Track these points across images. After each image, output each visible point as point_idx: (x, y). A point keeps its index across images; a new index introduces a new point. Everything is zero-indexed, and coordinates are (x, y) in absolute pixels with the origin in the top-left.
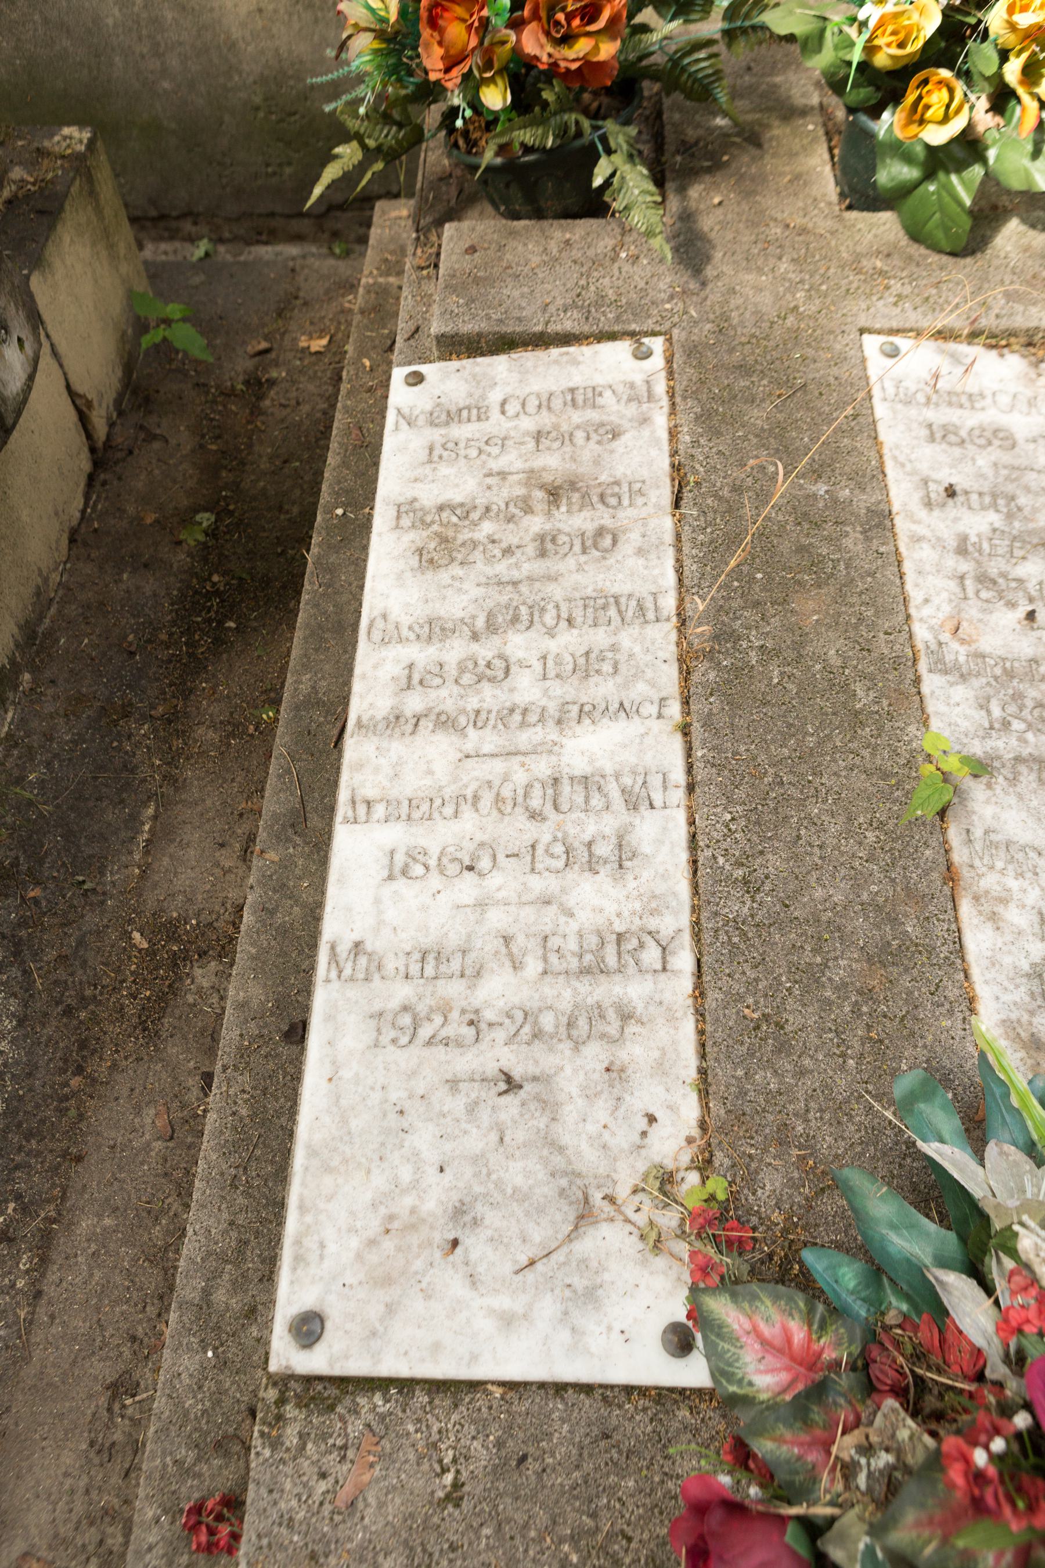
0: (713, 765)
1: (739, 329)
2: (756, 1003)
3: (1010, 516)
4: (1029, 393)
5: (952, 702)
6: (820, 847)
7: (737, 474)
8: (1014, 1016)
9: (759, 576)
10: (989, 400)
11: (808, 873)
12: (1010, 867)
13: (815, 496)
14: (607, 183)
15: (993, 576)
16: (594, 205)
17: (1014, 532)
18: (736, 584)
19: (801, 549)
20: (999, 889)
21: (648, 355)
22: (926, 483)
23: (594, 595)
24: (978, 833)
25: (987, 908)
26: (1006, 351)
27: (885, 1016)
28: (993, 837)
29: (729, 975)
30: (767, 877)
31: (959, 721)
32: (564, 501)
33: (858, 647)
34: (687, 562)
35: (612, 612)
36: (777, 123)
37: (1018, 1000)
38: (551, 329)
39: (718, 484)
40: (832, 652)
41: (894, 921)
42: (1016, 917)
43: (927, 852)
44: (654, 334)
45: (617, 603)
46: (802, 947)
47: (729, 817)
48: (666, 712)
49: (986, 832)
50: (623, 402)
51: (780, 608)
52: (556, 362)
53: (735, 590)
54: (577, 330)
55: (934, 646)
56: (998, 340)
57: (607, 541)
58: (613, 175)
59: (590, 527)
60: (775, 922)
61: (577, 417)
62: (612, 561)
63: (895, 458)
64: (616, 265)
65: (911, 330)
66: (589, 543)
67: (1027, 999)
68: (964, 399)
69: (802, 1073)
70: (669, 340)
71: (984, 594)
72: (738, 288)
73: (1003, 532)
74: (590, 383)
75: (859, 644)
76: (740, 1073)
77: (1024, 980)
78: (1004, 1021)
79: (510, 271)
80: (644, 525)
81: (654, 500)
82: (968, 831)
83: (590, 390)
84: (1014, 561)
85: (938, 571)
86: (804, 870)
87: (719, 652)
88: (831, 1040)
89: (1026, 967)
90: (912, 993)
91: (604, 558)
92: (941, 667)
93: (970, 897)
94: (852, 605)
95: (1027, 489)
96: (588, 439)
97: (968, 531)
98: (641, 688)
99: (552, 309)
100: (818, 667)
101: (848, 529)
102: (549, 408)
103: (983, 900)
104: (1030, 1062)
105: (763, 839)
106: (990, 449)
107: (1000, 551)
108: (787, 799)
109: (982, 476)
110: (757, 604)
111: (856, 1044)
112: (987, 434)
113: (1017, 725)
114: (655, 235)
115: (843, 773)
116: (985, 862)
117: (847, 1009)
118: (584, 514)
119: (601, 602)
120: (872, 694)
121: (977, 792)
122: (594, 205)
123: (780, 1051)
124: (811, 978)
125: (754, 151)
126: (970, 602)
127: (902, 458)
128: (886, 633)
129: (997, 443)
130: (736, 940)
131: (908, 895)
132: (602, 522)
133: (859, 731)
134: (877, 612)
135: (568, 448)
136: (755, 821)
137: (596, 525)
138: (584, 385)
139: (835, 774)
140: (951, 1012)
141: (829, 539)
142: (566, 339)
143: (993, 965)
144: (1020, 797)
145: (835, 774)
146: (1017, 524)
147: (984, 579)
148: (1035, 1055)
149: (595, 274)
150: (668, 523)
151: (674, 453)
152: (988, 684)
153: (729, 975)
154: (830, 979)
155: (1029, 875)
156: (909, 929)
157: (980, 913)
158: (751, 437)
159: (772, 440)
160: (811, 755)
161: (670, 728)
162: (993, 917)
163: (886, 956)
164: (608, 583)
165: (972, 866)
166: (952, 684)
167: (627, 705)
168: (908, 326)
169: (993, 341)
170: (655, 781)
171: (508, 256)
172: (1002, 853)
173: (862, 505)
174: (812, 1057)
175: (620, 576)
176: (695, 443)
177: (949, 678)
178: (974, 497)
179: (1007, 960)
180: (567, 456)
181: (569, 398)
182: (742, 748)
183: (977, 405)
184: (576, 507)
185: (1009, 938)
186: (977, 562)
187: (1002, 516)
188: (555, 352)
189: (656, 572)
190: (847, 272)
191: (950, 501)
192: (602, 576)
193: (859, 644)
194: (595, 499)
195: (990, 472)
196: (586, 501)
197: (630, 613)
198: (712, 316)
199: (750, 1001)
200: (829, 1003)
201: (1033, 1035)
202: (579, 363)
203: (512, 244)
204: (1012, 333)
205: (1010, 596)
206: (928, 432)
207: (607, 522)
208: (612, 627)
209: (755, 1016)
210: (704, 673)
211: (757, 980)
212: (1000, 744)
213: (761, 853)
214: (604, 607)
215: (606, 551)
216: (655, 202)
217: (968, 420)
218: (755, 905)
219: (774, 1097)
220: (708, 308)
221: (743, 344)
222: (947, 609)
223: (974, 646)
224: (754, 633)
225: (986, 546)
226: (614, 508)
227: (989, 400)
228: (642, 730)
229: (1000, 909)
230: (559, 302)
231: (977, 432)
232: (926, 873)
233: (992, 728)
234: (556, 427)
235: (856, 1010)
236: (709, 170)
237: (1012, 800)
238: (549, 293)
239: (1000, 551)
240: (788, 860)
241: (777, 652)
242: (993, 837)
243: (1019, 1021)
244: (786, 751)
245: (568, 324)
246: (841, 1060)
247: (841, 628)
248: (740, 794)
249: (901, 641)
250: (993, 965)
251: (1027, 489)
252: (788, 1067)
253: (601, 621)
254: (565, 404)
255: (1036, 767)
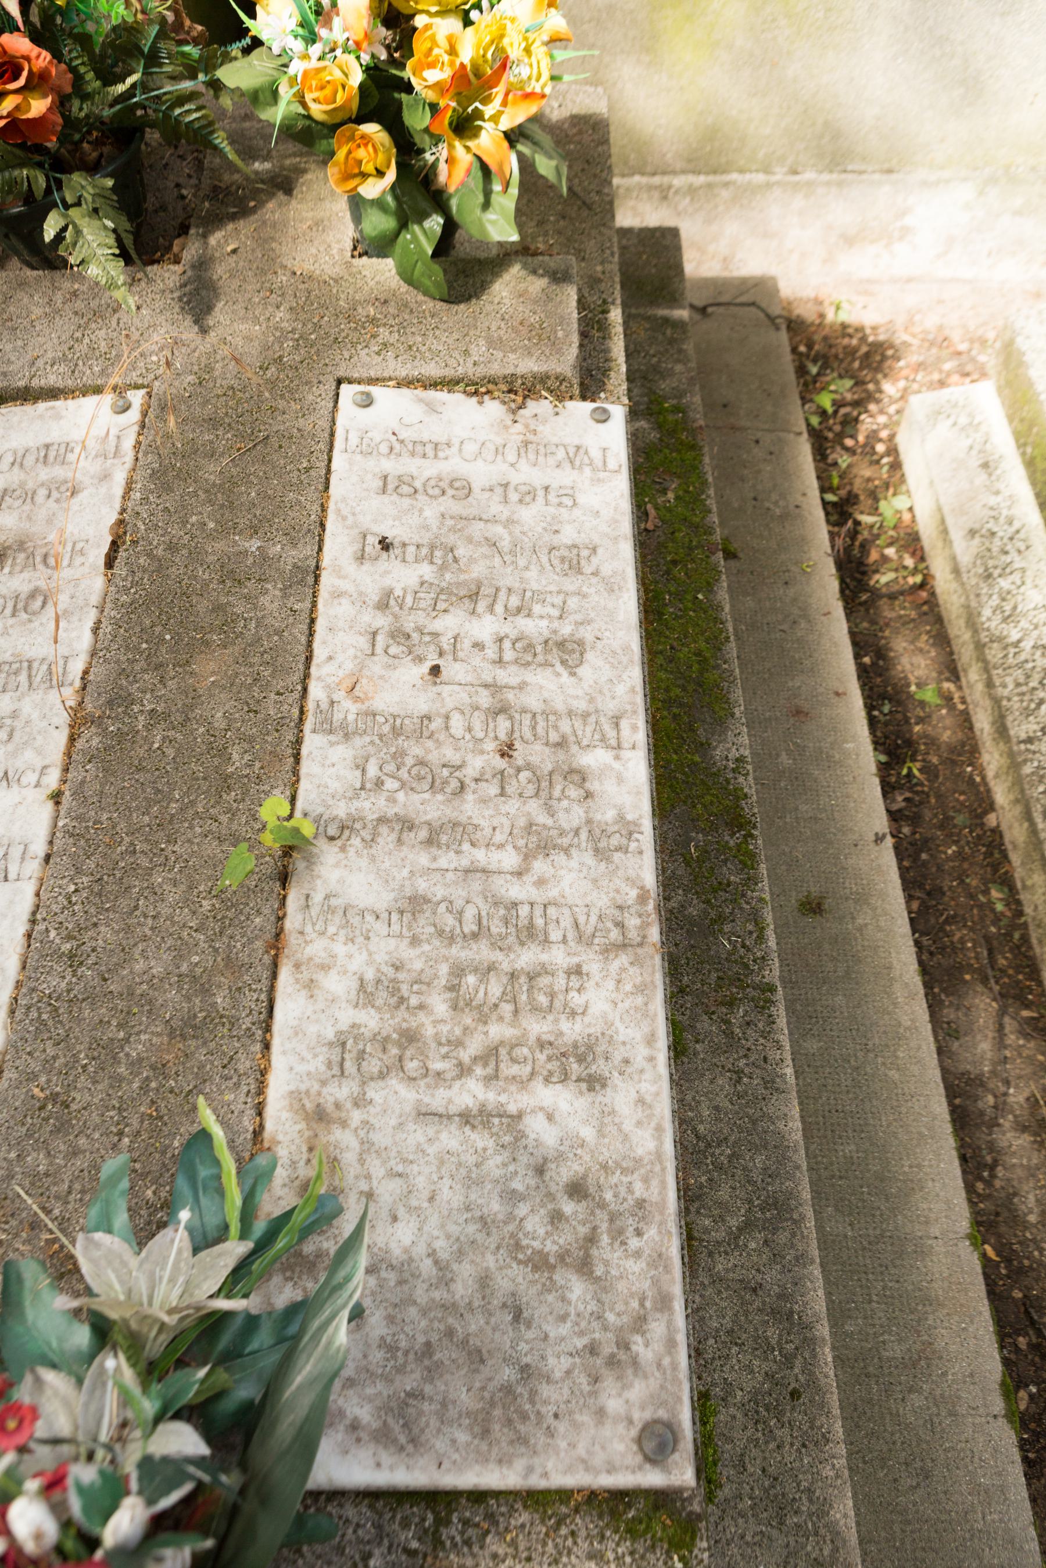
0: (72, 835)
1: (219, 381)
2: (49, 1081)
3: (443, 568)
4: (499, 441)
5: (328, 762)
6: (154, 917)
7: (175, 531)
8: (303, 1087)
9: (168, 637)
10: (455, 449)
11: (135, 945)
12: (342, 932)
13: (245, 553)
14: (59, 238)
15: (408, 630)
16: (50, 259)
17: (444, 584)
18: (144, 646)
19: (218, 608)
20: (323, 955)
21: (126, 408)
22: (365, 536)
23: (11, 659)
24: (317, 898)
25: (305, 975)
26: (486, 397)
27: (171, 1092)
28: (334, 902)
29: (29, 1053)
30: (93, 950)
31: (329, 781)
32: (9, 562)
33: (246, 709)
34: (105, 623)
35: (23, 678)
36: (313, 166)
37: (313, 1070)
38: (35, 383)
39: (155, 543)
40: (219, 715)
41: (205, 991)
42: (337, 984)
43: (257, 920)
44: (137, 387)
45: (30, 668)
46: (109, 1022)
47: (72, 888)
48: (45, 780)
49: (327, 897)
50: (90, 458)
51: (180, 670)
52: (41, 417)
53: (141, 653)
54: (60, 384)
55: (324, 706)
56: (478, 388)
57: (39, 600)
58: (64, 229)
59: (25, 589)
60: (90, 998)
61: (44, 474)
62: (36, 624)
63: (338, 511)
64: (116, 316)
65: (390, 379)
66: (20, 605)
67: (323, 1068)
68: (429, 450)
69: (75, 1152)
70: (149, 395)
71: (393, 650)
72: (229, 338)
73: (431, 584)
74: (66, 439)
75: (248, 704)
76: (13, 1155)
77: (325, 1049)
78: (292, 1092)
79: (9, 324)
80: (76, 586)
81: (91, 560)
82: (308, 896)
83: (63, 446)
84: (435, 614)
85: (351, 627)
86: (132, 942)
87: (109, 717)
88: (112, 1118)
89: (330, 1034)
90: (204, 1066)
91: (30, 621)
92: (327, 727)
93: (291, 964)
94: (252, 665)
95: (470, 540)
96: (49, 496)
97: (394, 584)
98: (29, 756)
99: (40, 363)
100: (202, 730)
101: (269, 586)
102: (21, 465)
103: (303, 968)
104: (307, 1134)
105: (101, 910)
106: (441, 499)
107: (423, 604)
108: (135, 867)
109: (427, 528)
110: (159, 666)
111: (135, 1122)
112: (444, 484)
113: (390, 784)
114: (118, 287)
115: (196, 841)
116: (317, 928)
117: (135, 1085)
118: (26, 575)
119: (15, 666)
120: (247, 757)
121: (328, 855)
122: (50, 259)
123: (59, 1131)
124: (107, 1053)
125: (281, 196)
126: (375, 658)
127: (344, 512)
128: (278, 694)
129: (450, 492)
130: (45, 1016)
131: (226, 966)
132: (39, 583)
133: (225, 796)
134: (274, 671)
135: (27, 507)
136: (98, 890)
137: (31, 587)
138: (59, 440)
139: (189, 841)
140: (237, 1085)
141: (247, 598)
142: (53, 394)
143: (296, 1034)
144: (373, 859)
145: (189, 841)
146: (448, 576)
147: (399, 635)
148: (315, 1126)
149: (93, 326)
150: (98, 583)
151: (123, 511)
152: (372, 742)
153: (29, 1053)
154: (127, 1055)
155: (360, 939)
156: (219, 1001)
157: (297, 981)
158: (200, 493)
159: (219, 495)
160: (171, 822)
161: (44, 797)
162: (310, 985)
163: (186, 1029)
164: (26, 647)
165: (302, 933)
166: (332, 744)
167: (10, 774)
168: (386, 375)
169: (472, 389)
170: (16, 852)
171: (12, 309)
172: (338, 919)
173: (290, 561)
174: (88, 1136)
175: (40, 639)
176: (145, 500)
177: (332, 738)
178: (411, 549)
179: (312, 1029)
180: (24, 516)
181: (42, 454)
182: (105, 816)
183: (441, 454)
184: (18, 568)
185: (321, 1005)
186: (396, 616)
187: (434, 568)
188: (42, 406)
189: (74, 634)
190: (341, 319)
191: (385, 554)
192: (23, 640)
193: (248, 704)
194: (38, 559)
195: (434, 523)
196: (30, 563)
197: (38, 678)
198: (196, 368)
199: (43, 1079)
200: (120, 1079)
201: (318, 1105)
202: (61, 418)
203: (20, 294)
204: (492, 381)
205: (419, 651)
206: (381, 484)
207: (42, 584)
208: (18, 693)
209: (42, 1095)
210: (91, 739)
211: (55, 1058)
212: (367, 805)
213: (95, 925)
214: (16, 673)
215: (34, 613)
216: (114, 255)
217: (424, 470)
218: (74, 980)
219: (40, 1180)
220: (194, 360)
221: (218, 396)
222: (349, 666)
223: (367, 704)
224: (148, 696)
225: (409, 600)
226: (52, 568)
227: (455, 449)
228: (17, 800)
229: (319, 976)
230: (50, 355)
231: (433, 483)
232: (250, 941)
233: (362, 788)
234: (22, 484)
235: (144, 1088)
236: (234, 217)
237: (364, 863)
238: (41, 346)
239: (423, 604)
240: (118, 932)
241: (166, 716)
242: (334, 902)
243: (307, 1092)
244: (147, 818)
245: (52, 379)
246: (116, 1138)
247: (235, 689)
248: (90, 864)
249: (290, 701)
250: (296, 1034)
251: (470, 540)
252: (62, 1147)
253: (10, 687)
254: (37, 460)
255: (398, 827)
